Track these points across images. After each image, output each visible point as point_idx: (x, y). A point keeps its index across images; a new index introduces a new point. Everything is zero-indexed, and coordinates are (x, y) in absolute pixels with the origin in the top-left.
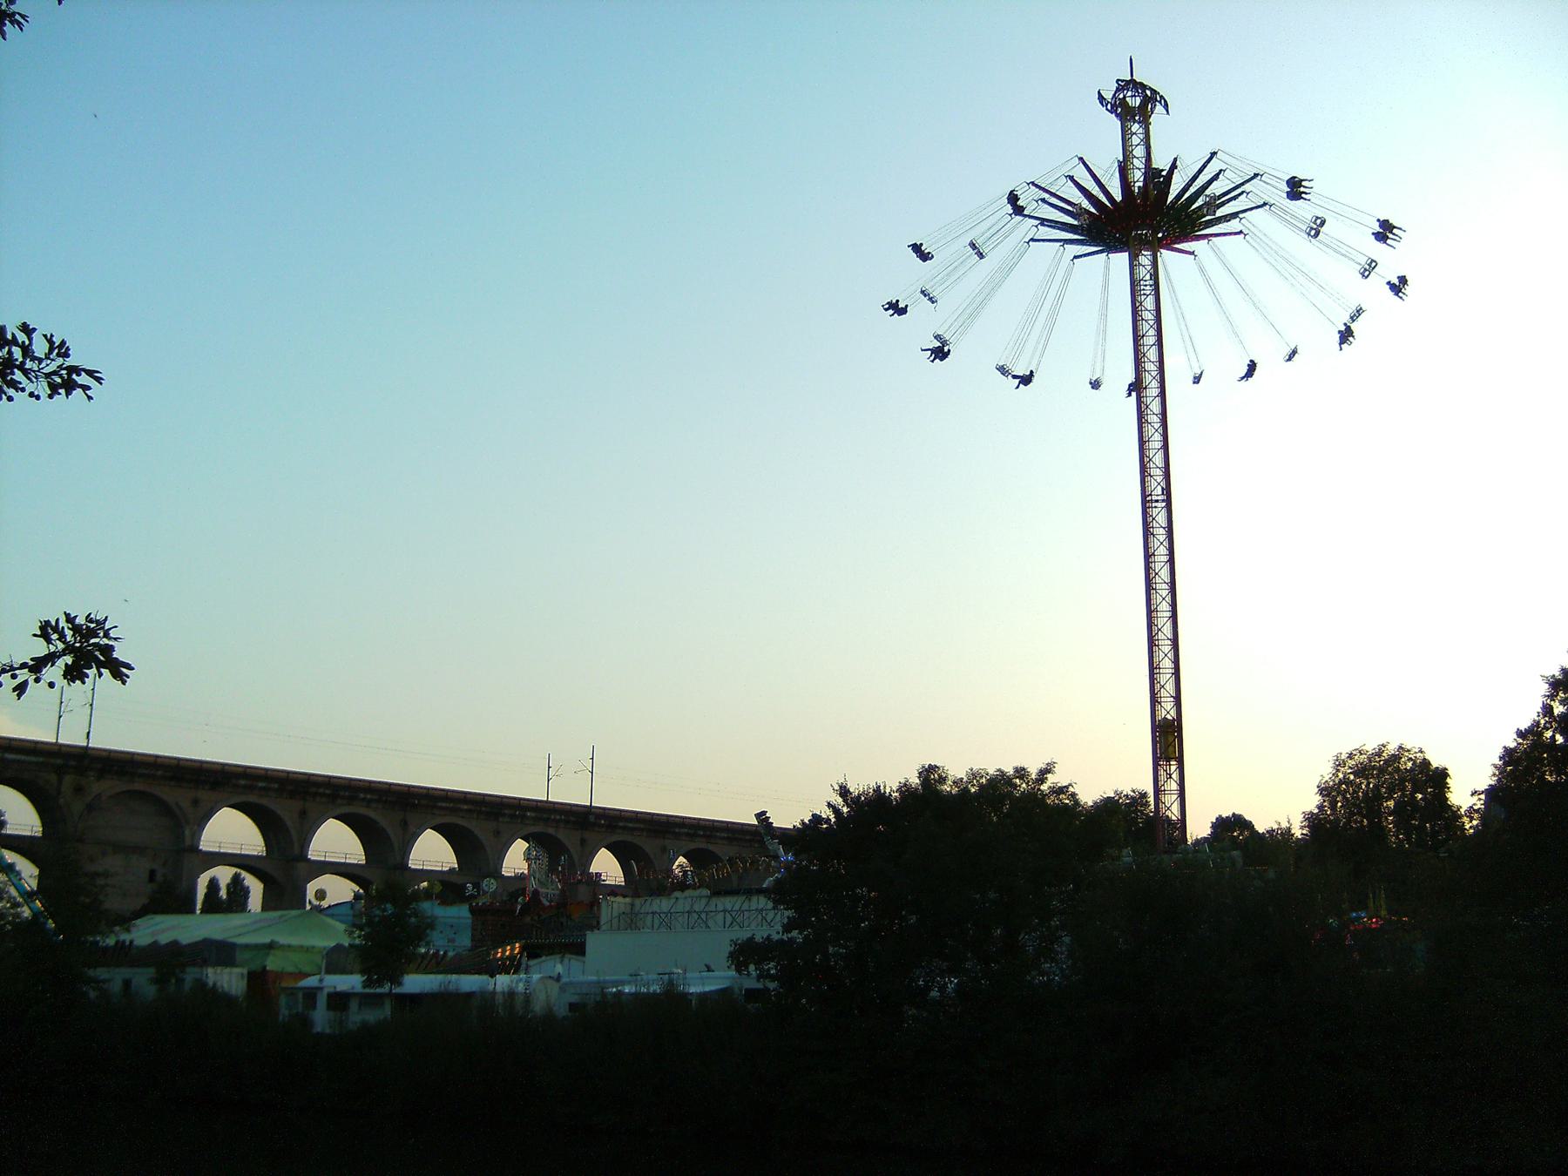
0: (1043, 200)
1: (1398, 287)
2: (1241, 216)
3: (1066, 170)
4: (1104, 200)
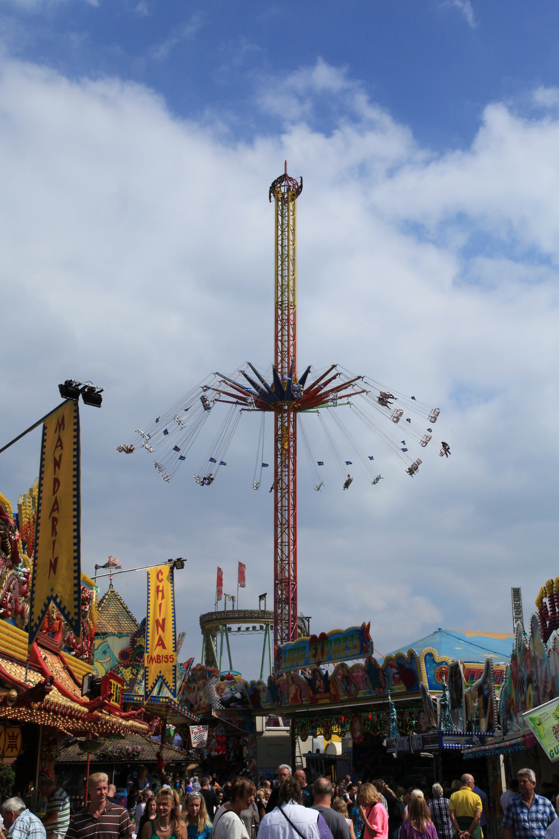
2: (353, 383)
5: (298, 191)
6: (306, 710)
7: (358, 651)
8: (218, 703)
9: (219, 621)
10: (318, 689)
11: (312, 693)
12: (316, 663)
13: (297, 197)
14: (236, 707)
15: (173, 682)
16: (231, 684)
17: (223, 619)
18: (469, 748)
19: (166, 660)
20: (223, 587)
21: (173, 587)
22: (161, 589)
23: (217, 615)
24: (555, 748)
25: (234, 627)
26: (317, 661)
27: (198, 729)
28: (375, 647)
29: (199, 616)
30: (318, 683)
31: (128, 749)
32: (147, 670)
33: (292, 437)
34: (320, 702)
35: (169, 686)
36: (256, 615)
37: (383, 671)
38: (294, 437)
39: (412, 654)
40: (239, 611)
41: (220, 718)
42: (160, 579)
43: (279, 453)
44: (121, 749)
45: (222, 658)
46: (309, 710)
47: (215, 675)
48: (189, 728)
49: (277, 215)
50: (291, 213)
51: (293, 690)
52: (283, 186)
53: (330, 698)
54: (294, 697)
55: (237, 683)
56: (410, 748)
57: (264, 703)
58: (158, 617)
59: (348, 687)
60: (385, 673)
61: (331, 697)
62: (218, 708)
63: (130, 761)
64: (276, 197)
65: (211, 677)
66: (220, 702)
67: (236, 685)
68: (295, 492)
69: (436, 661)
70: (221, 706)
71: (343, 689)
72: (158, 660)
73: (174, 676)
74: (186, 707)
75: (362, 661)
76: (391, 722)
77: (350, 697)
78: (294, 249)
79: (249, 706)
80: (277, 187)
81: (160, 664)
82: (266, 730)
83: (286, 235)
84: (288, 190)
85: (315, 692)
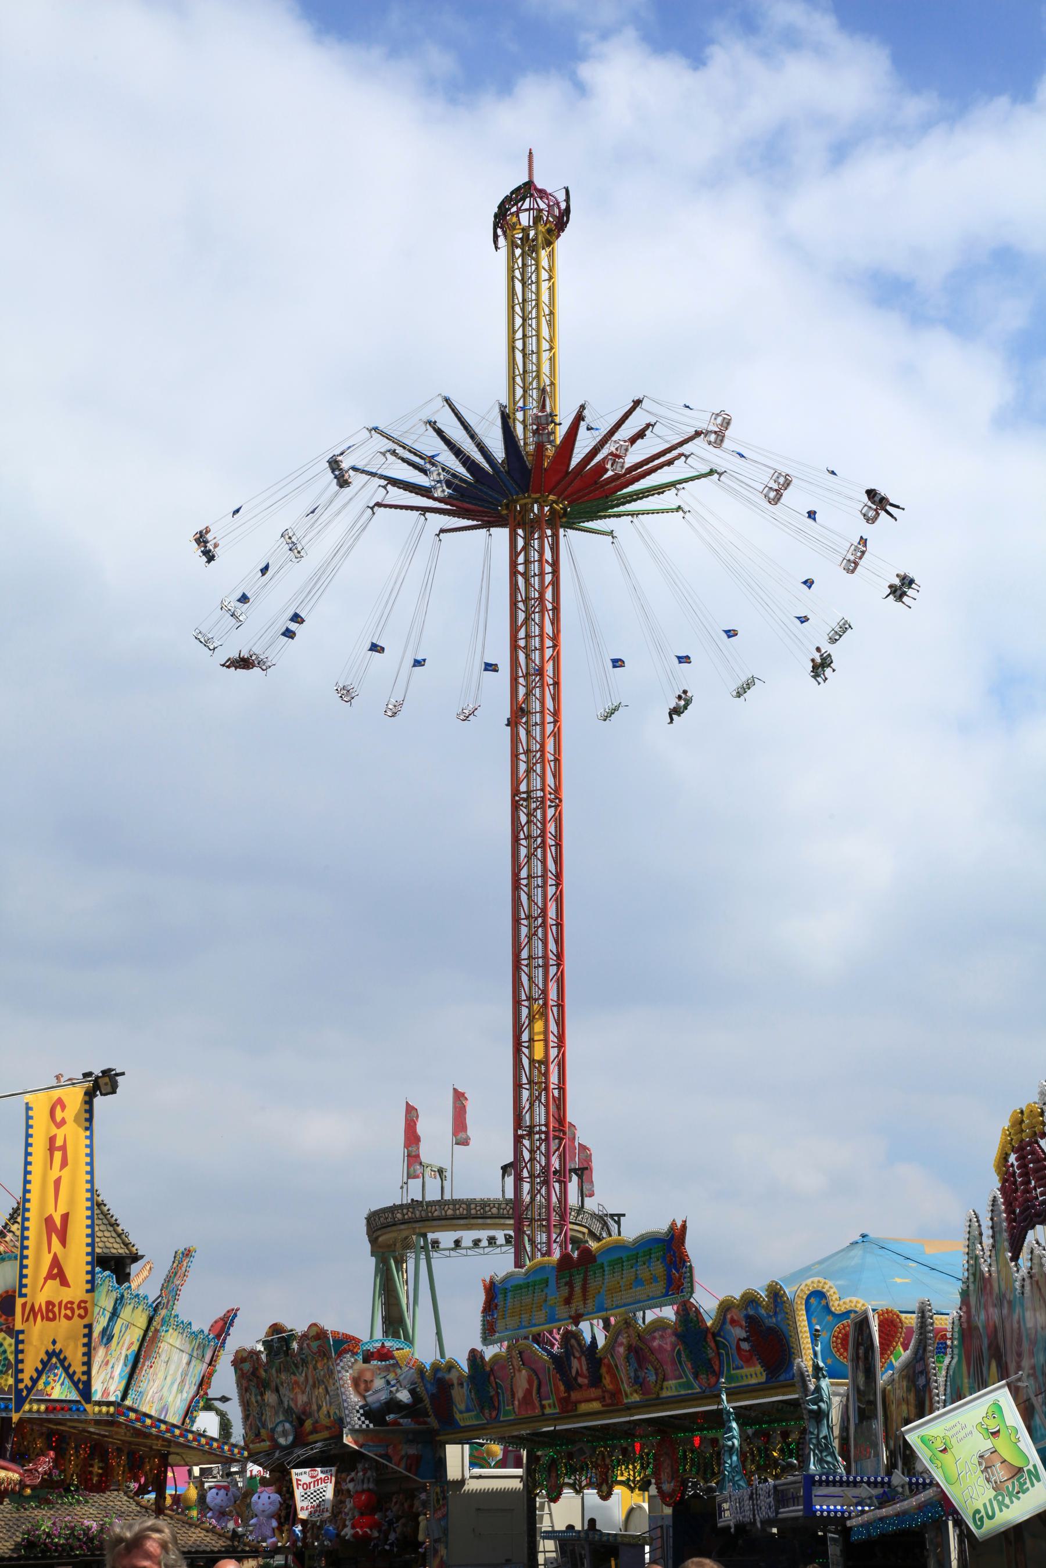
0: (394, 453)
1: (903, 587)
3: (426, 415)
4: (485, 465)
5: (561, 222)
6: (552, 1428)
7: (659, 1287)
8: (359, 1415)
9: (410, 1225)
10: (576, 1379)
11: (562, 1388)
12: (570, 1317)
13: (558, 236)
14: (399, 1424)
15: (84, 1364)
16: (387, 1369)
17: (418, 1221)
18: (863, 1512)
19: (69, 1312)
20: (422, 1145)
21: (91, 1138)
22: (59, 1143)
23: (405, 1211)
24: (985, 1505)
25: (446, 1238)
26: (573, 1313)
27: (312, 1477)
28: (698, 1277)
29: (365, 1214)
30: (575, 1363)
31: (89, 1528)
32: (21, 1337)
33: (553, 796)
34: (584, 1407)
35: (74, 1372)
36: (495, 1210)
37: (717, 1333)
38: (556, 798)
39: (775, 1293)
40: (455, 1203)
41: (362, 1450)
42: (58, 1119)
43: (522, 836)
44: (73, 1529)
45: (417, 1309)
46: (558, 1428)
47: (350, 1350)
48: (290, 1474)
49: (512, 278)
50: (544, 275)
51: (522, 1381)
52: (526, 210)
53: (601, 1399)
54: (524, 1397)
55: (401, 1368)
56: (754, 1515)
57: (461, 1412)
58: (50, 1210)
59: (641, 1374)
60: (719, 1339)
61: (604, 1397)
62: (357, 1427)
63: (93, 1555)
64: (509, 238)
65: (340, 1354)
66: (361, 1411)
67: (399, 1371)
68: (559, 925)
69: (833, 1309)
70: (363, 1422)
71: (630, 1378)
72: (50, 1312)
73: (85, 1349)
74: (287, 1426)
75: (669, 1313)
76: (727, 1455)
77: (647, 1397)
78: (552, 360)
79: (429, 1420)
80: (512, 214)
81: (53, 1324)
82: (471, 1477)
83: (534, 326)
84: (537, 219)
85: (571, 1384)
